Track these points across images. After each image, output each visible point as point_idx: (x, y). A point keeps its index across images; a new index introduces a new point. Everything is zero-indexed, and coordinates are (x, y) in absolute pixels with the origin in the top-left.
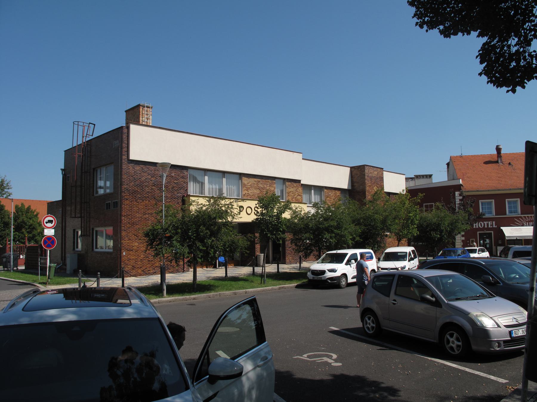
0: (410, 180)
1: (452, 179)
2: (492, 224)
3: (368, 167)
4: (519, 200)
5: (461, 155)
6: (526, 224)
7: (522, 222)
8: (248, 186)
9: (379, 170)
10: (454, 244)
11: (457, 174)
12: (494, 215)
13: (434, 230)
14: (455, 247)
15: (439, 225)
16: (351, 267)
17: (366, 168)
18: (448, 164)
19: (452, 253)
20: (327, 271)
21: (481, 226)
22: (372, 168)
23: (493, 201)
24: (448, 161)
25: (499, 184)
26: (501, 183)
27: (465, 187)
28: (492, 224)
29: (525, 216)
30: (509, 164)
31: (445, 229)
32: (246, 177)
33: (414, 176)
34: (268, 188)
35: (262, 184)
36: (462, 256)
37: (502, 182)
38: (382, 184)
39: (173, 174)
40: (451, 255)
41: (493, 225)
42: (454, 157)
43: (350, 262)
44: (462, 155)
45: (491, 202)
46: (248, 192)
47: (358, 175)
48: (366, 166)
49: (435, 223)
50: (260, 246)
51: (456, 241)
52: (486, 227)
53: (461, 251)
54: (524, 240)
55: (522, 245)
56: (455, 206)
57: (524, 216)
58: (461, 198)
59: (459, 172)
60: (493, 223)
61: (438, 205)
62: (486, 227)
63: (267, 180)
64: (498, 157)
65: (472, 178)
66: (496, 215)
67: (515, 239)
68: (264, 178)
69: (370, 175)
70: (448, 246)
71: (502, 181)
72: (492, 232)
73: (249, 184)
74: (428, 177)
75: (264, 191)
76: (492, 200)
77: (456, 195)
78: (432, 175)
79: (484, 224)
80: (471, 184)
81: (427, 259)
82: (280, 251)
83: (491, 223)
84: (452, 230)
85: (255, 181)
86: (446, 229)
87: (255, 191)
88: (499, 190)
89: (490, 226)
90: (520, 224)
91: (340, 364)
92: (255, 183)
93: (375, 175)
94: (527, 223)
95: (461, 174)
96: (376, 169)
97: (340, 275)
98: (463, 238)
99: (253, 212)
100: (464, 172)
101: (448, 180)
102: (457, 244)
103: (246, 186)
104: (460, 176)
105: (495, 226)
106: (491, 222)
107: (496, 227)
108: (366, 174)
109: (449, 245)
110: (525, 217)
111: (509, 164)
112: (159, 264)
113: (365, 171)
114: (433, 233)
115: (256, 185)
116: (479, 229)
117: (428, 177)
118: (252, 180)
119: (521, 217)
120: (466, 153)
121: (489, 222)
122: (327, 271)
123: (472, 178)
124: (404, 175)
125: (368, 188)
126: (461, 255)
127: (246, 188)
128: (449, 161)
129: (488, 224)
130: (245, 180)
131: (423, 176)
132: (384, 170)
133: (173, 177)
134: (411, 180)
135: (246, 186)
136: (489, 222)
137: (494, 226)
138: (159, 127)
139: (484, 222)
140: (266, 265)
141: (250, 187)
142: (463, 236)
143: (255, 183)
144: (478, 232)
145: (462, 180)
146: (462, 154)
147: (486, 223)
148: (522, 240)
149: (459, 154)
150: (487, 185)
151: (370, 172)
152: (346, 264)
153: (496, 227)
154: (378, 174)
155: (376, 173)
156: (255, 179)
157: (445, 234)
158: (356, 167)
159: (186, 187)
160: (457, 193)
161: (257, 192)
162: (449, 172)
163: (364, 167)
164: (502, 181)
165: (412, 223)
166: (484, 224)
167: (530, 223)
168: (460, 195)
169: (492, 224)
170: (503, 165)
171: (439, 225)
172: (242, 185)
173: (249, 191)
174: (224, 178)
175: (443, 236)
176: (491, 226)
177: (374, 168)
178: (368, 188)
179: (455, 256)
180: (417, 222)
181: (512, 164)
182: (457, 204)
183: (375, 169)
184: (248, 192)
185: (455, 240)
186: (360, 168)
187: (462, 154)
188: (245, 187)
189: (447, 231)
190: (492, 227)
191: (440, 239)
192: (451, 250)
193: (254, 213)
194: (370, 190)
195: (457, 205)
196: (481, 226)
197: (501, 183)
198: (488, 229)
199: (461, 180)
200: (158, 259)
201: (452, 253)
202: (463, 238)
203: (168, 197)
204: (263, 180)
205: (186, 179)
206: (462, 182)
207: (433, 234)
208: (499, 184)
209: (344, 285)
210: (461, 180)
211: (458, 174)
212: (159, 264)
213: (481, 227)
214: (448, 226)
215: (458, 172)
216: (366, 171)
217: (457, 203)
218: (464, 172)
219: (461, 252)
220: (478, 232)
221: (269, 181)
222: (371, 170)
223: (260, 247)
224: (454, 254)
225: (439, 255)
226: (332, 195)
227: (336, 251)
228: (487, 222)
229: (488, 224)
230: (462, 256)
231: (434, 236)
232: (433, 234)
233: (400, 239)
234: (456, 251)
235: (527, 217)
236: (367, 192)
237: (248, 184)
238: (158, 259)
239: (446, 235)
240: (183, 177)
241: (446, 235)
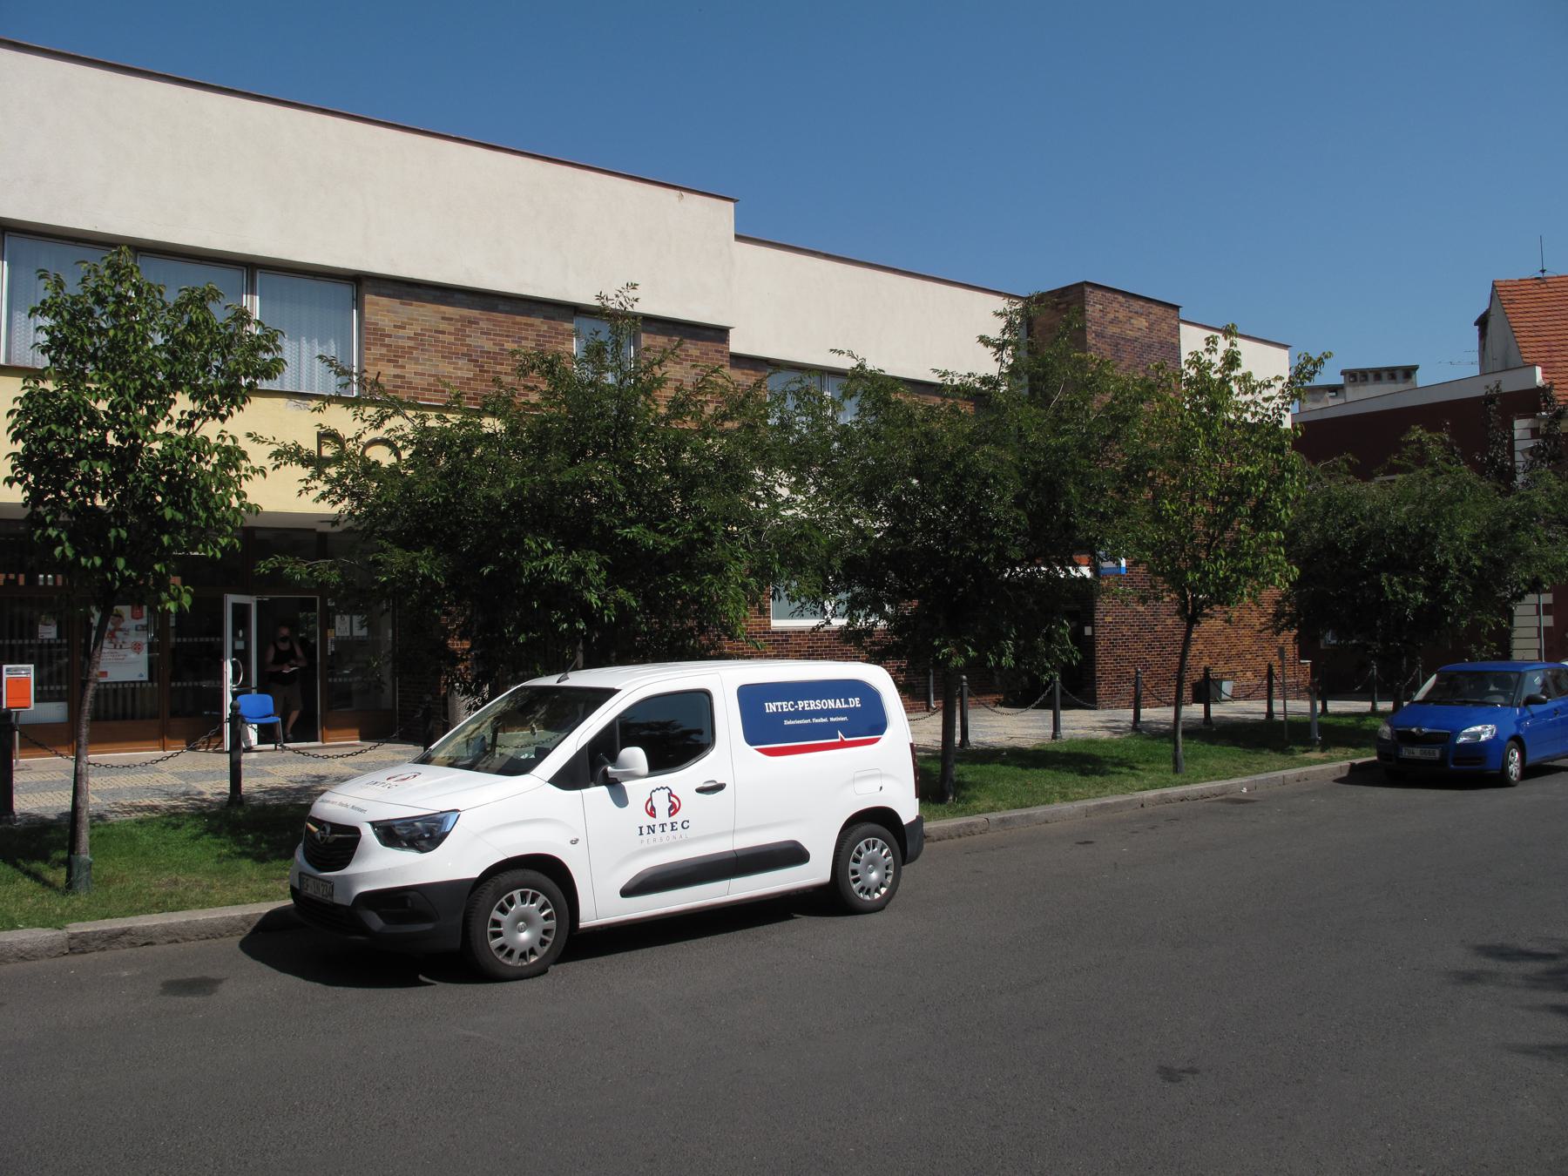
0: (1328, 394)
3: (1099, 293)
5: (1540, 275)
8: (401, 342)
9: (1156, 310)
10: (1503, 642)
11: (1518, 340)
13: (1394, 565)
14: (1507, 655)
15: (1425, 539)
16: (620, 799)
17: (1093, 297)
18: (1483, 322)
19: (1492, 688)
20: (368, 833)
22: (1121, 298)
24: (1483, 307)
31: (1458, 561)
32: (389, 296)
33: (1343, 373)
35: (485, 334)
36: (1552, 704)
40: (1486, 699)
42: (1510, 284)
43: (613, 759)
44: (1546, 274)
46: (398, 371)
48: (1088, 289)
49: (1403, 530)
51: (1516, 619)
53: (1545, 674)
56: (1513, 460)
59: (1530, 339)
61: (1419, 440)
63: (519, 319)
68: (500, 307)
70: (1473, 648)
73: (409, 332)
74: (1399, 374)
77: (1517, 435)
78: (1415, 368)
81: (1374, 708)
84: (1497, 568)
85: (443, 318)
86: (1463, 559)
92: (443, 326)
93: (1138, 334)
95: (1540, 349)
96: (1143, 307)
97: (473, 871)
98: (1548, 621)
100: (1553, 338)
101: (1483, 373)
102: (1516, 644)
103: (387, 340)
104: (1536, 355)
108: (1089, 325)
109: (1480, 646)
114: (1390, 581)
117: (1399, 374)
118: (427, 314)
122: (368, 833)
124: (1285, 347)
126: (1544, 702)
127: (384, 351)
128: (1486, 306)
130: (381, 310)
131: (1378, 374)
132: (1183, 314)
134: (1334, 394)
135: (387, 340)
141: (411, 343)
142: (1548, 609)
143: (443, 326)
145: (1543, 373)
146: (1543, 271)
149: (1532, 272)
151: (1111, 316)
152: (568, 779)
154: (1150, 328)
155: (1142, 323)
156: (443, 308)
157: (1454, 588)
160: (1521, 426)
161: (459, 373)
162: (1488, 349)
163: (1083, 292)
165: (1261, 516)
171: (1425, 539)
172: (364, 331)
173: (404, 367)
174: (253, 293)
175: (1447, 599)
177: (1132, 302)
179: (1511, 705)
180: (1286, 514)
182: (1522, 452)
183: (1137, 305)
184: (398, 371)
185: (1511, 622)
187: (1543, 271)
189: (1466, 571)
191: (1431, 618)
192: (1486, 672)
195: (1518, 457)
199: (1539, 370)
201: (1492, 688)
202: (1548, 621)
204: (500, 317)
206: (1544, 378)
207: (1391, 585)
209: (532, 951)
210: (1539, 370)
211: (1524, 350)
214: (1473, 546)
215: (1523, 339)
216: (1093, 311)
217: (1519, 446)
218: (1553, 338)
219: (1544, 684)
221: (537, 321)
222: (1118, 309)
224: (1505, 695)
225: (1420, 696)
227: (557, 677)
230: (1552, 704)
231: (1395, 594)
232: (1391, 584)
233: (1194, 609)
234: (1514, 677)
237: (401, 332)
239: (1465, 591)
241: (1465, 591)
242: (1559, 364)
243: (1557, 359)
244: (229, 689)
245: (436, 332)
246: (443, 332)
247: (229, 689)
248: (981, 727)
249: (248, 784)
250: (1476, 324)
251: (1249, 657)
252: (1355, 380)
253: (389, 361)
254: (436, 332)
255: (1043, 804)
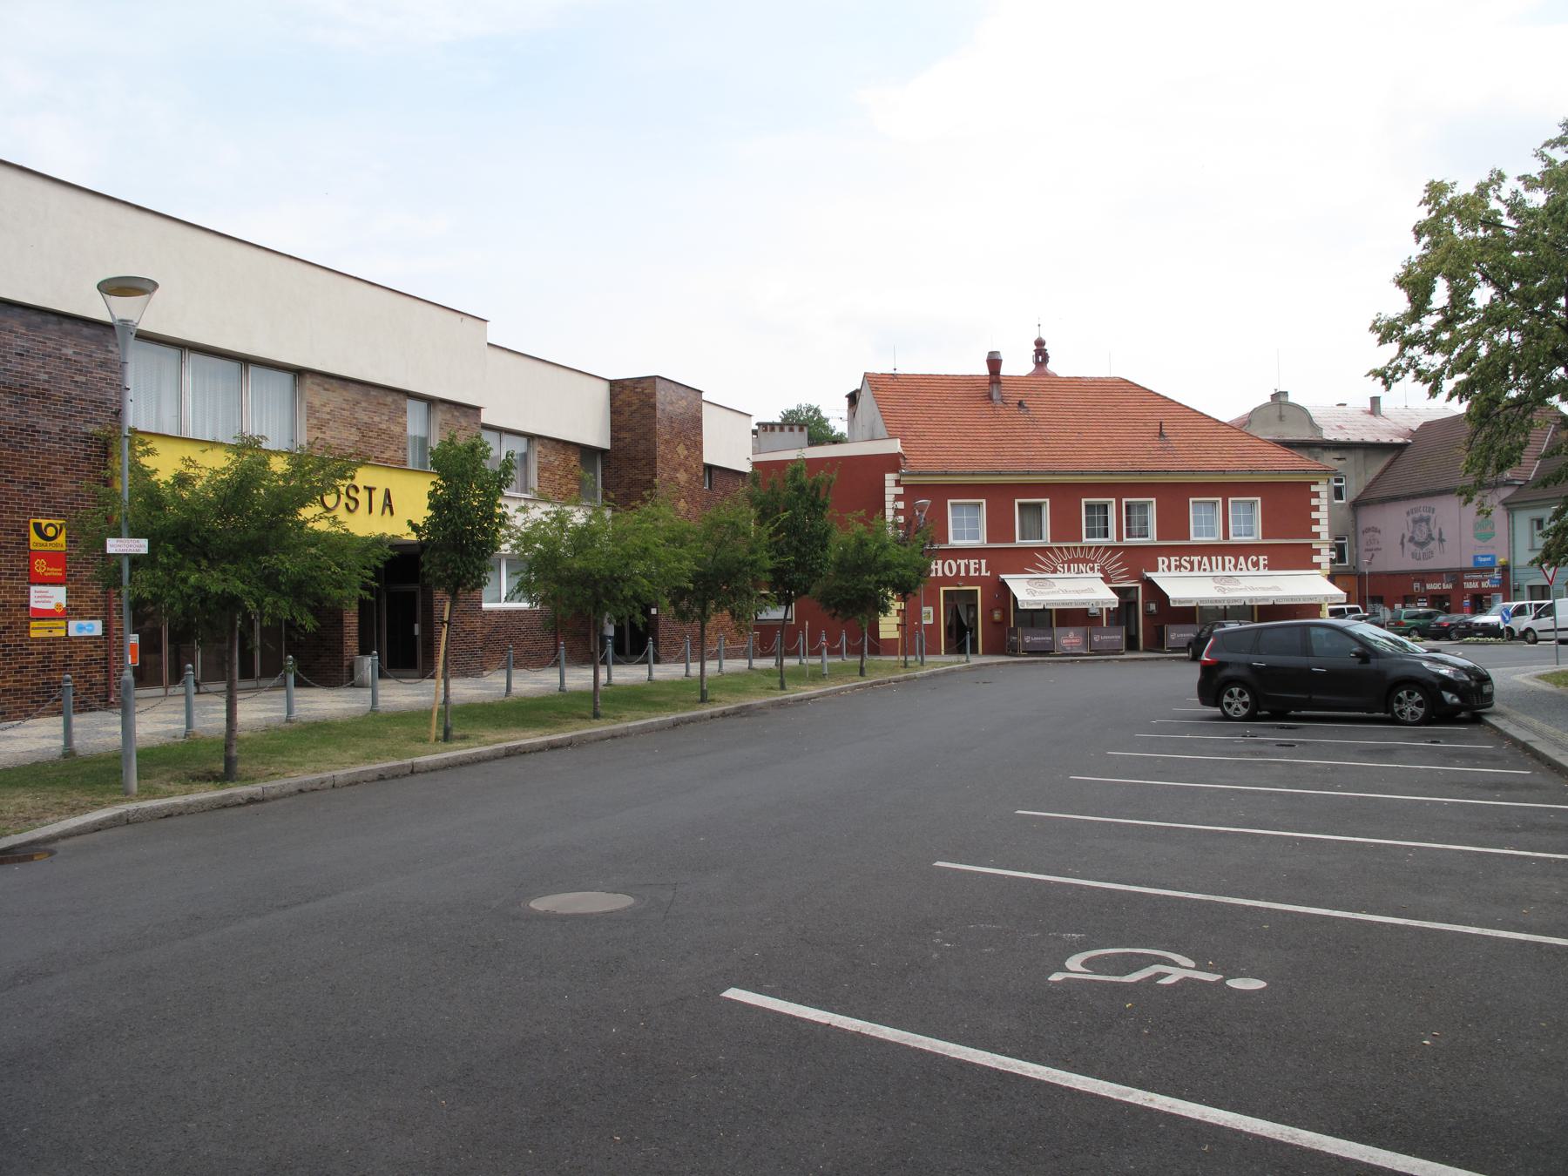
1: (867, 436)
2: (977, 566)
3: (663, 382)
4: (1048, 503)
5: (893, 372)
6: (1063, 568)
7: (1053, 561)
12: (1155, 539)
21: (951, 571)
23: (982, 503)
25: (999, 457)
26: (1002, 454)
27: (912, 461)
28: (1178, 563)
29: (1062, 547)
30: (1020, 404)
34: (384, 426)
37: (1007, 454)
38: (698, 439)
39: (69, 352)
41: (979, 570)
44: (897, 372)
45: (1039, 507)
47: (634, 407)
48: (657, 380)
50: (359, 620)
52: (963, 573)
54: (1057, 610)
55: (1253, 621)
57: (1057, 547)
58: (900, 491)
60: (980, 564)
62: (963, 573)
64: (991, 383)
65: (927, 438)
66: (1263, 538)
67: (1041, 607)
69: (669, 408)
71: (1005, 450)
72: (979, 588)
73: (327, 409)
75: (371, 434)
76: (1257, 498)
79: (959, 567)
80: (927, 453)
82: (416, 637)
83: (975, 564)
85: (344, 400)
87: (345, 434)
88: (1000, 474)
89: (972, 573)
90: (1048, 566)
91: (1260, 984)
92: (345, 406)
94: (1066, 565)
99: (342, 505)
105: (987, 572)
106: (977, 561)
107: (989, 574)
110: (1060, 549)
111: (1020, 404)
112: (15, 681)
113: (655, 394)
115: (346, 413)
116: (945, 580)
119: (1050, 549)
120: (903, 369)
121: (972, 562)
123: (927, 438)
125: (662, 447)
127: (315, 422)
129: (967, 567)
133: (70, 360)
136: (970, 561)
137: (983, 573)
138: (20, 164)
139: (959, 561)
140: (381, 683)
141: (328, 417)
144: (942, 589)
147: (962, 563)
148: (1051, 610)
150: (968, 457)
153: (989, 574)
158: (627, 383)
159: (117, 401)
160: (890, 478)
161: (352, 437)
163: (655, 382)
164: (1005, 450)
166: (959, 567)
167: (1072, 565)
168: (898, 483)
169: (979, 568)
170: (1002, 406)
173: (324, 433)
176: (975, 572)
178: (662, 447)
181: (1026, 405)
186: (642, 385)
188: (315, 418)
190: (977, 574)
193: (347, 505)
194: (668, 453)
196: (951, 571)
197: (1002, 454)
198: (969, 580)
200: (11, 664)
203: (50, 433)
205: (117, 373)
208: (999, 457)
212: (15, 681)
213: (950, 575)
218: (905, 419)
220: (942, 589)
223: (359, 623)
226: (557, 463)
228: (1199, 558)
229: (967, 567)
235: (1056, 550)
236: (658, 460)
238: (11, 664)
240: (103, 364)
242: (909, 438)
243: (908, 434)
244: (1526, 593)
245: (341, 409)
246: (344, 410)
247: (1526, 593)
248: (305, 702)
249: (591, 672)
250: (846, 396)
251: (727, 629)
252: (766, 430)
253: (318, 428)
254: (341, 409)
255: (351, 774)
